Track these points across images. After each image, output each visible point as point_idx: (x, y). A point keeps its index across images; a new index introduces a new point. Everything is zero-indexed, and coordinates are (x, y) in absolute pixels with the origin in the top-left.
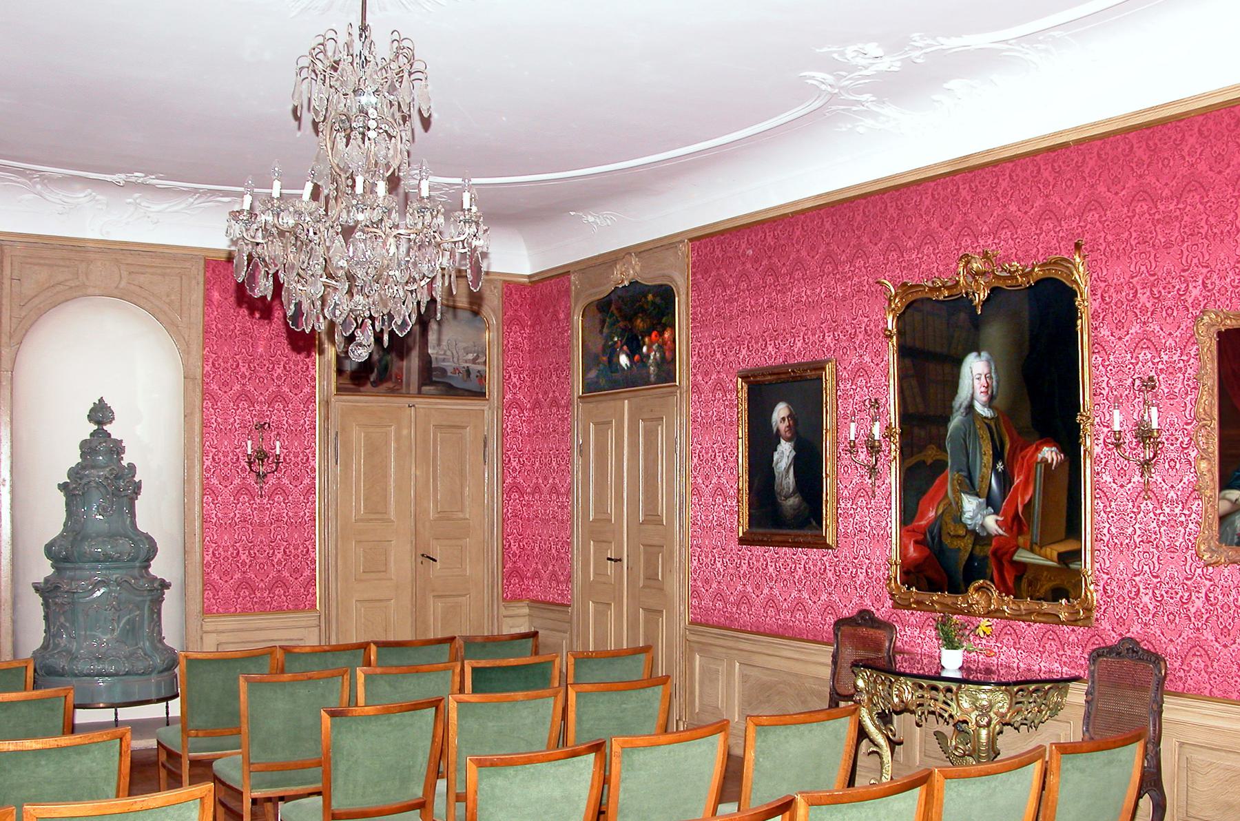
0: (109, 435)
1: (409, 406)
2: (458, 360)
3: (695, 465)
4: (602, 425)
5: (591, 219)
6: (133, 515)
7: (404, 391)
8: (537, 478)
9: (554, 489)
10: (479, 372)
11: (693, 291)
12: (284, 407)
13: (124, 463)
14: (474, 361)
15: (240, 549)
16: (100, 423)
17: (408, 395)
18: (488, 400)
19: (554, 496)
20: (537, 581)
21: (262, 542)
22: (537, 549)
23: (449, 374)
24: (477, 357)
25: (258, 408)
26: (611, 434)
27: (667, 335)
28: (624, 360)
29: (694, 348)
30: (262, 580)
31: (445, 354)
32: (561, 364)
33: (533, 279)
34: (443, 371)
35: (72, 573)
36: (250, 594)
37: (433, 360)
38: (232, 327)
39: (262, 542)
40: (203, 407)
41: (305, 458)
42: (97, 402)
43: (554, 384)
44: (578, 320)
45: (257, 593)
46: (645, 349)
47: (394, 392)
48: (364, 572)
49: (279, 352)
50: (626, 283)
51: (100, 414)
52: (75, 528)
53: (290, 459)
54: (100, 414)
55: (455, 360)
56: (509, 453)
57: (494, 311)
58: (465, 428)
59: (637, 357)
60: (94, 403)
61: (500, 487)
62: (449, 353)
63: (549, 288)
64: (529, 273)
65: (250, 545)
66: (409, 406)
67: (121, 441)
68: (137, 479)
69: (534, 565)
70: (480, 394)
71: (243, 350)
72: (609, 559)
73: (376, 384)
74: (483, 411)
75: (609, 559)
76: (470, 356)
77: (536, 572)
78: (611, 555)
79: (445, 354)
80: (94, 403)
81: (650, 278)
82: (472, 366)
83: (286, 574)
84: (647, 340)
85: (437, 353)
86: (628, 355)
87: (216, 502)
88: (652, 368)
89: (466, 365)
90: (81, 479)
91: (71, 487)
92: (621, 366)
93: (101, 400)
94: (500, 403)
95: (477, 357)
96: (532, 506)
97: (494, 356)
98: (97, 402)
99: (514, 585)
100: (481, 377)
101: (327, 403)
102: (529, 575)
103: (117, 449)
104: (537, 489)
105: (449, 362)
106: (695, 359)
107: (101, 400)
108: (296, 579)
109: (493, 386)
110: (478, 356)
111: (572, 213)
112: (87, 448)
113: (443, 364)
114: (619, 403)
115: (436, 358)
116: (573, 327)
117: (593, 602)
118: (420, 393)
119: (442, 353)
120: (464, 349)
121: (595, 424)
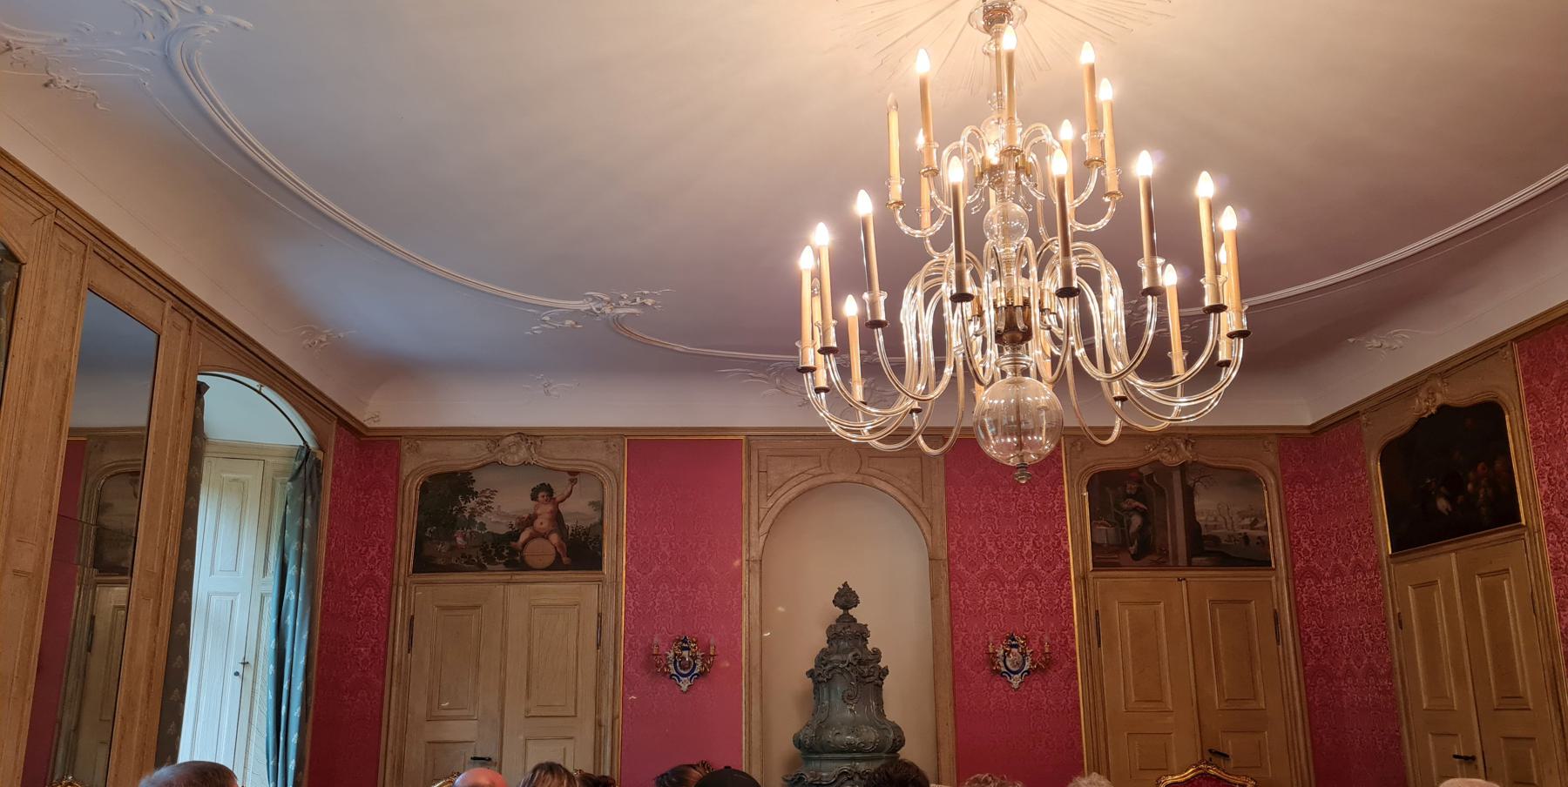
0: (855, 620)
1: (1179, 580)
2: (1233, 526)
3: (1546, 492)
4: (1426, 586)
5: (1375, 343)
6: (880, 703)
7: (1171, 563)
8: (1336, 559)
9: (1358, 566)
10: (1259, 538)
11: (1528, 403)
12: (1037, 585)
13: (870, 647)
14: (1252, 526)
15: (987, 540)
16: (846, 608)
17: (1176, 567)
18: (1273, 569)
19: (1360, 576)
20: (1350, 681)
21: (1009, 533)
22: (1346, 642)
23: (1223, 542)
24: (1256, 522)
25: (1008, 588)
26: (1438, 596)
27: (1498, 465)
28: (1442, 504)
29: (1541, 476)
30: (1005, 477)
31: (1216, 520)
32: (1360, 521)
33: (1314, 430)
34: (1216, 539)
35: (818, 764)
36: (999, 587)
37: (1203, 528)
38: (981, 602)
39: (1009, 533)
40: (950, 589)
41: (1063, 640)
42: (842, 587)
43: (1355, 545)
44: (1376, 468)
45: (1006, 585)
46: (1470, 486)
47: (1160, 564)
48: (1141, 769)
49: (1027, 528)
50: (1433, 411)
51: (846, 598)
52: (820, 720)
53: (1040, 543)
54: (846, 598)
55: (1229, 526)
56: (1308, 630)
57: (1271, 469)
58: (1249, 602)
59: (1460, 498)
60: (839, 588)
61: (1301, 671)
62: (1220, 519)
63: (1347, 533)
64: (1309, 423)
65: (997, 536)
66: (1179, 580)
67: (866, 625)
68: (882, 664)
69: (1344, 662)
70: (1262, 561)
71: (989, 528)
72: (1455, 757)
73: (1136, 557)
74: (1270, 582)
75: (1455, 757)
76: (1247, 521)
77: (1337, 568)
78: (1459, 750)
79: (1216, 520)
80: (839, 588)
81: (1461, 393)
82: (1249, 532)
83: (1036, 566)
84: (1471, 475)
85: (1206, 520)
86: (1447, 498)
87: (963, 588)
88: (1483, 509)
89: (1243, 531)
90: (825, 665)
91: (816, 674)
92: (1439, 511)
93: (845, 585)
94: (1290, 574)
95: (1256, 522)
96: (1323, 496)
97: (1274, 517)
98: (842, 587)
99: (1310, 587)
100: (1263, 542)
101: (1084, 578)
102: (1327, 574)
103: (862, 634)
104: (1338, 571)
105: (1222, 528)
106: (1545, 487)
107: (845, 585)
108: (1049, 572)
109: (1278, 550)
110: (1256, 520)
111: (1351, 340)
112: (833, 635)
113: (1214, 532)
114: (1443, 558)
115: (1206, 526)
116: (1370, 475)
117: (1432, 734)
118: (1190, 564)
119: (1213, 519)
120: (1239, 513)
121: (1415, 587)
